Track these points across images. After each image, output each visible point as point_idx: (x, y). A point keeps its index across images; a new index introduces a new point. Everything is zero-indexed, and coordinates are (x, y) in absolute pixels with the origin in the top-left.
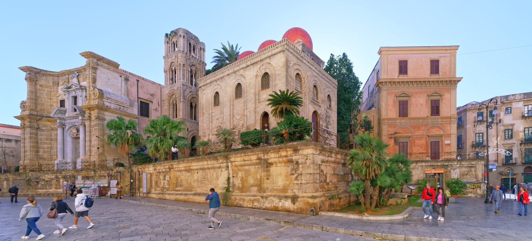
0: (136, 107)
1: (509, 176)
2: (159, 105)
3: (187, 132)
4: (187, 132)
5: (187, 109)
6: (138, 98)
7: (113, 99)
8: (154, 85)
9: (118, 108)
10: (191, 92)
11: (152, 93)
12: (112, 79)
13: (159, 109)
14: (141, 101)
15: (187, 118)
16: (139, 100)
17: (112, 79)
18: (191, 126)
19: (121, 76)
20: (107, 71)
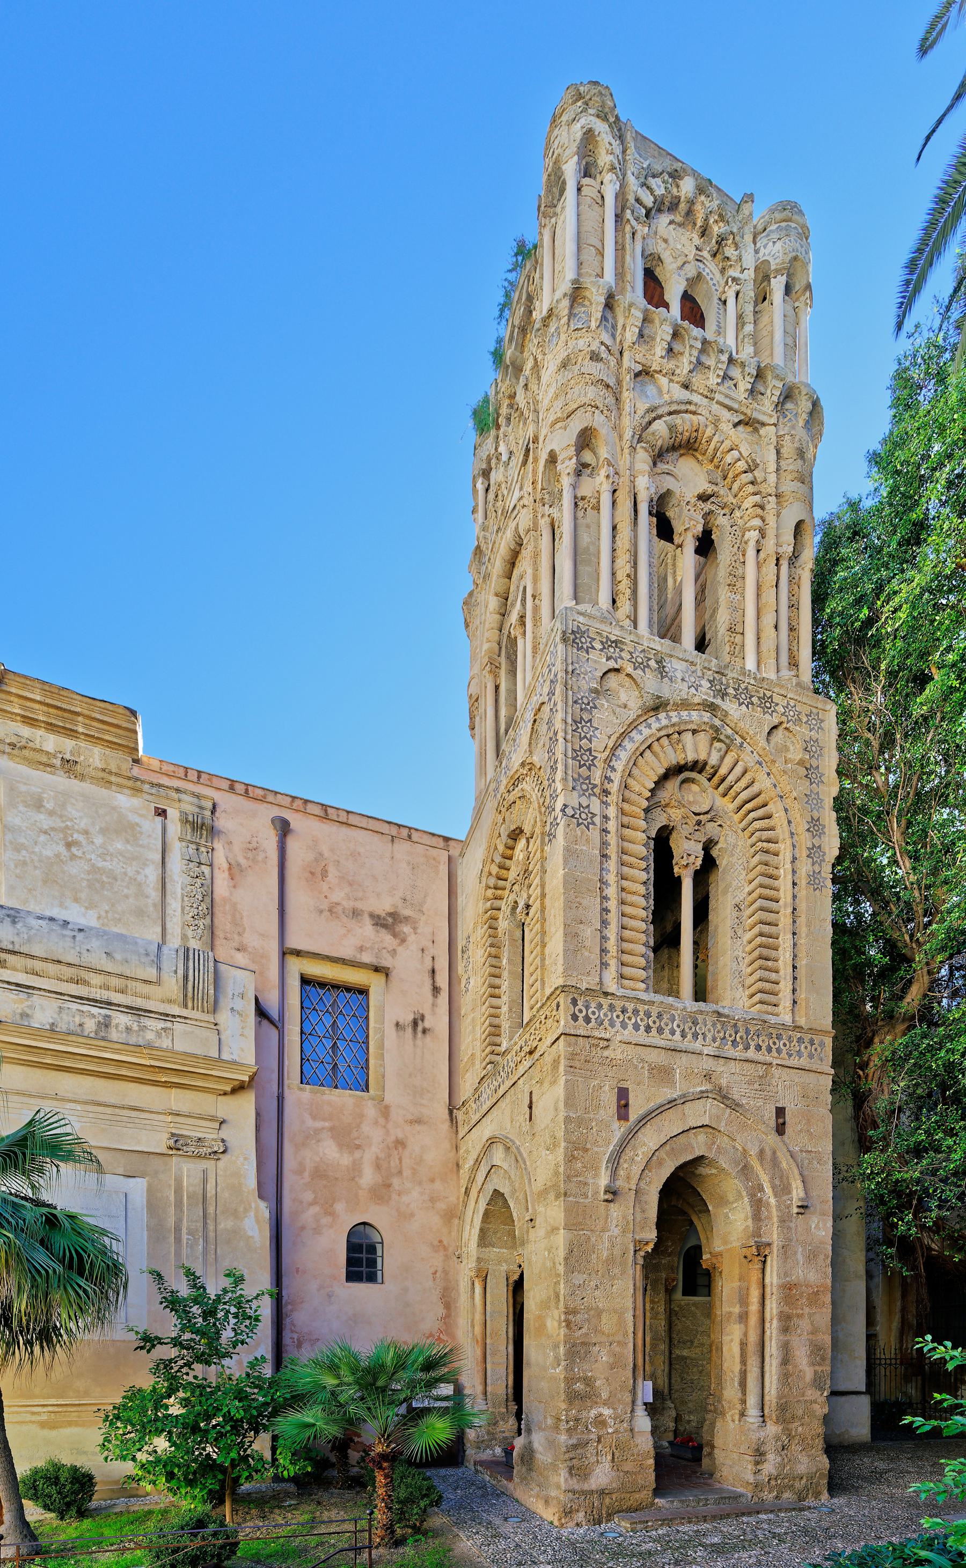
0: (239, 1004)
1: (367, 1259)
2: (436, 990)
3: (618, 1130)
4: (618, 1130)
5: (611, 891)
6: (285, 953)
7: (37, 950)
8: (402, 848)
9: (90, 1026)
10: (658, 706)
11: (384, 906)
12: (98, 840)
13: (438, 1021)
14: (305, 981)
15: (612, 987)
16: (296, 967)
17: (98, 840)
18: (654, 1057)
19: (162, 813)
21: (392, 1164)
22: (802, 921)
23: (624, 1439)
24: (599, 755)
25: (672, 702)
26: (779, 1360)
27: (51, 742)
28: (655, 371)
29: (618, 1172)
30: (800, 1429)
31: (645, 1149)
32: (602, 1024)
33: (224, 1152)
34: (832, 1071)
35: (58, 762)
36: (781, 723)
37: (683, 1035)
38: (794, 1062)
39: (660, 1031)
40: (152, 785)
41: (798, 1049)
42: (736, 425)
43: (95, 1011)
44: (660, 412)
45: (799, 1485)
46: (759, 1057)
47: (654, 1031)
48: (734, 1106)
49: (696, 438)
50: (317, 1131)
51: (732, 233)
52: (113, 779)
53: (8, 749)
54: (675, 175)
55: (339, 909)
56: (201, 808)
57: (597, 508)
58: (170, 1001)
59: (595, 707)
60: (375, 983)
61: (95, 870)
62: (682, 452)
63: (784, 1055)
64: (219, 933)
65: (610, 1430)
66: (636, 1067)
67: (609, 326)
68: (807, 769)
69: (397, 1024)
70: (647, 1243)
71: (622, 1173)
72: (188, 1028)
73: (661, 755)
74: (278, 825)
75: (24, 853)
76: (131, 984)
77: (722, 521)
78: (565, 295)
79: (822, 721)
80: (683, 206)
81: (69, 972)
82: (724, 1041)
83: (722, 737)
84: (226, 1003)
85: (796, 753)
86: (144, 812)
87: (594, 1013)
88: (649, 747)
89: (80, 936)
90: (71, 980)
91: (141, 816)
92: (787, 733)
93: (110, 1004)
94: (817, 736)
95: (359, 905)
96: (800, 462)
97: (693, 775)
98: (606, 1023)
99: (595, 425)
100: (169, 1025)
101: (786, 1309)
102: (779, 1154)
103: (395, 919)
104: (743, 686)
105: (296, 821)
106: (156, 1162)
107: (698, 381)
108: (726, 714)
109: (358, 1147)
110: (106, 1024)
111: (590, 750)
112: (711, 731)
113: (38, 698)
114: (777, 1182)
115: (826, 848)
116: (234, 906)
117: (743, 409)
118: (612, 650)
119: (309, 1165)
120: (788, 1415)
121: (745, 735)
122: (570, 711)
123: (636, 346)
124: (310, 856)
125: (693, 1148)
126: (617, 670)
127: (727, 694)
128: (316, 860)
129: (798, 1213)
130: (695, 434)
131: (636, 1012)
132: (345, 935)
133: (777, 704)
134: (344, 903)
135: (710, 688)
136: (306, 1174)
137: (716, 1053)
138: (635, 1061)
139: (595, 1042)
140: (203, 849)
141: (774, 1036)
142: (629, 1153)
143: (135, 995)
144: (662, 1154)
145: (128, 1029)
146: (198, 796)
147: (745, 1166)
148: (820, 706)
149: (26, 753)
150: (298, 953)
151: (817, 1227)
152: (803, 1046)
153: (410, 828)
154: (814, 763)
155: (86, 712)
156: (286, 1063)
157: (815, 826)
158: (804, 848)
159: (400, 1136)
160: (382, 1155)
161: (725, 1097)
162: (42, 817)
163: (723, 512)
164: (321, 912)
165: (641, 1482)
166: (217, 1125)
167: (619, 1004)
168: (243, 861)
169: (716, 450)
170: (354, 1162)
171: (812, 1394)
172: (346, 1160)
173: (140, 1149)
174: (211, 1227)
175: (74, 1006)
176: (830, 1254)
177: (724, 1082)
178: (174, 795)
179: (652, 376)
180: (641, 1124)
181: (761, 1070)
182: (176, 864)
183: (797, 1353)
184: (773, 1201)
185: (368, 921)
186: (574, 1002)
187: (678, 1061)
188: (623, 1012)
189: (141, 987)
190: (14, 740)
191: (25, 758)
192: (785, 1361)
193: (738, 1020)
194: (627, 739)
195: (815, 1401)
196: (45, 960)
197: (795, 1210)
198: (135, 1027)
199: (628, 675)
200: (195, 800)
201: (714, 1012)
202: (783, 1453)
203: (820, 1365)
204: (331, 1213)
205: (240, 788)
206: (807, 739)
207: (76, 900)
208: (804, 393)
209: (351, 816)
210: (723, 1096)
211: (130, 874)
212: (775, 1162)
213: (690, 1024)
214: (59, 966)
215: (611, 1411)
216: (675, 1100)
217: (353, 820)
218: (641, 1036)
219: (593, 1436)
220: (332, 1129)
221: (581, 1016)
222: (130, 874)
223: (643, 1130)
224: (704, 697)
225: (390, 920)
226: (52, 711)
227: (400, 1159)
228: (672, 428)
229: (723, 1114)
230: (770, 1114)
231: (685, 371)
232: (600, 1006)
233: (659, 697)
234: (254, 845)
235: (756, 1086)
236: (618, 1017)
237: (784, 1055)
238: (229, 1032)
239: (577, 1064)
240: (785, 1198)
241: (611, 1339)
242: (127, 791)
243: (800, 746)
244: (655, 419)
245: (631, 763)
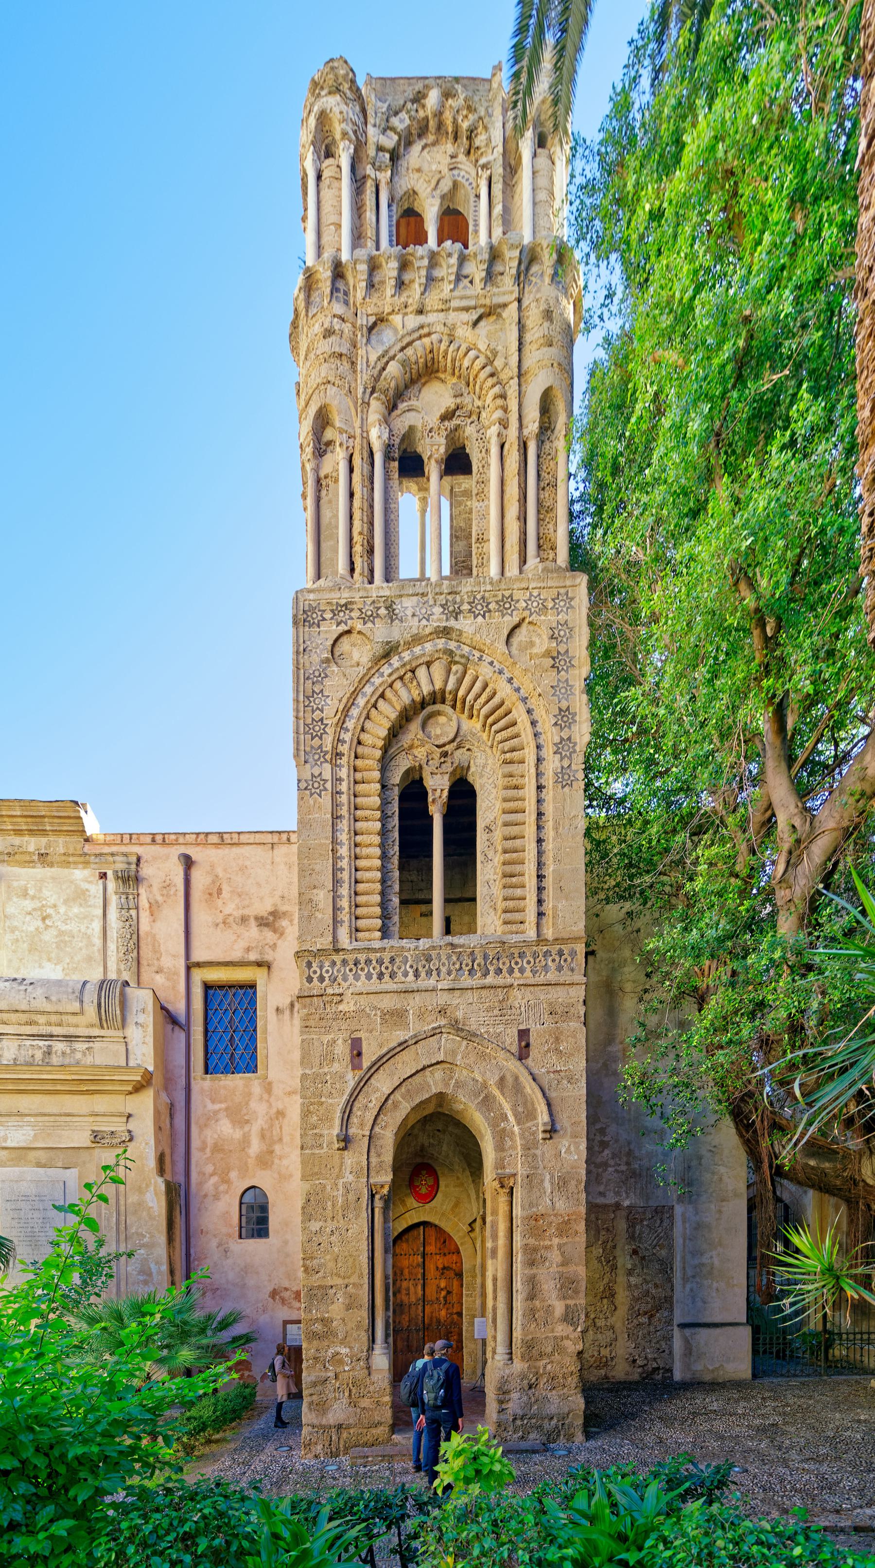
0: (141, 1018)
3: (351, 1079)
9: (39, 1055)
11: (263, 908)
18: (388, 1003)
20: (39, 871)
21: (274, 1133)
22: (549, 826)
23: (360, 1377)
24: (329, 722)
25: (402, 643)
26: (524, 1295)
27: (32, 844)
28: (389, 314)
29: (351, 1121)
30: (549, 1367)
31: (378, 1094)
32: (335, 980)
33: (131, 1140)
34: (584, 980)
35: (36, 858)
36: (523, 619)
37: (417, 975)
38: (541, 979)
39: (392, 976)
40: (96, 855)
41: (544, 963)
42: (475, 324)
43: (41, 1043)
44: (391, 353)
45: (547, 1426)
46: (499, 981)
47: (387, 977)
48: (470, 1036)
49: (433, 359)
50: (216, 1112)
51: (480, 118)
52: (71, 859)
53: (6, 858)
54: (419, 98)
55: (231, 919)
56: (129, 863)
57: (336, 481)
58: (92, 1026)
59: (326, 676)
60: (258, 976)
61: (61, 933)
62: (423, 381)
63: (528, 973)
64: (144, 962)
65: (347, 1368)
66: (369, 1016)
67: (341, 295)
68: (553, 658)
69: (278, 1009)
70: (382, 1186)
71: (355, 1120)
72: (104, 1045)
73: (394, 699)
74: (182, 859)
75: (17, 933)
76: (64, 1017)
77: (470, 431)
78: (300, 288)
79: (572, 599)
80: (432, 124)
81: (24, 1017)
82: (461, 972)
83: (457, 659)
84: (131, 1019)
85: (542, 644)
86: (92, 879)
87: (327, 971)
88: (382, 696)
89: (30, 988)
91: (90, 882)
92: (531, 628)
93: (52, 1036)
94: (566, 617)
95: (246, 912)
96: (546, 324)
97: (438, 707)
98: (339, 979)
99: (328, 401)
100: (91, 1044)
101: (532, 1241)
102: (522, 1079)
103: (275, 917)
104: (478, 597)
105: (194, 853)
106: (84, 1155)
107: (433, 300)
108: (461, 633)
109: (247, 1122)
110: (48, 1053)
111: (322, 720)
112: (445, 657)
113: (19, 813)
114: (520, 1109)
115: (576, 738)
116: (154, 937)
117: (482, 301)
118: (342, 614)
119: (210, 1142)
121: (482, 647)
122: (301, 689)
123: (367, 300)
124: (209, 880)
125: (429, 1086)
126: (349, 632)
127: (461, 612)
128: (214, 882)
129: (544, 1139)
130: (431, 356)
131: (368, 962)
132: (236, 941)
133: (518, 601)
134: (235, 913)
135: (443, 613)
136: (208, 1150)
137: (450, 987)
138: (367, 1009)
139: (329, 999)
140: (131, 897)
141: (516, 955)
142: (362, 1100)
143: (68, 1025)
144: (397, 1096)
145: (63, 1053)
146: (125, 855)
147: (486, 1097)
148: (568, 583)
149: (17, 857)
150: (198, 965)
151: (568, 1150)
152: (550, 959)
153: (288, 832)
154: (562, 648)
155: (48, 814)
156: (192, 1059)
157: (565, 717)
158: (551, 745)
159: (280, 1107)
160: (266, 1126)
161: (458, 1029)
162: (27, 902)
163: (469, 421)
164: (217, 925)
165: (377, 1418)
166: (125, 1119)
167: (351, 958)
168: (160, 899)
169: (454, 360)
170: (244, 1134)
171: (561, 1329)
172: (238, 1134)
173: (72, 1145)
174: (122, 1202)
175: (28, 1043)
176: (584, 1178)
177: (460, 1015)
178: (111, 859)
179: (387, 320)
180: (373, 1070)
181: (500, 993)
182: (113, 913)
183: (545, 1287)
184: (516, 1129)
185: (253, 923)
186: (309, 965)
187: (411, 1002)
188: (355, 965)
190: (10, 850)
191: (17, 861)
192: (531, 1297)
193: (474, 947)
194: (360, 695)
196: (8, 1011)
197: (541, 1136)
198: (68, 1051)
199: (359, 632)
200: (124, 859)
201: (447, 944)
202: (530, 1392)
203: (572, 1298)
204: (226, 1181)
205: (159, 838)
206: (554, 625)
207: (49, 960)
208: (545, 246)
209: (242, 836)
210: (457, 1027)
211: (83, 930)
212: (518, 1087)
213: (424, 962)
214: (18, 1014)
215: (348, 1350)
216: (406, 1041)
217: (244, 838)
218: (374, 985)
219: (331, 1374)
220: (227, 1109)
221: (315, 976)
222: (83, 930)
223: (375, 1076)
224: (435, 624)
225: (271, 918)
226: (29, 820)
227: (281, 1128)
228: (404, 363)
229: (460, 1045)
230: (511, 1039)
231: (417, 296)
232: (334, 963)
233: (388, 643)
234: (168, 882)
235: (496, 1012)
236: (351, 970)
237: (528, 973)
238: (134, 1042)
239: (311, 1023)
240: (529, 1124)
241: (346, 1281)
242: (80, 866)
243: (545, 634)
244: (387, 363)
245: (364, 716)
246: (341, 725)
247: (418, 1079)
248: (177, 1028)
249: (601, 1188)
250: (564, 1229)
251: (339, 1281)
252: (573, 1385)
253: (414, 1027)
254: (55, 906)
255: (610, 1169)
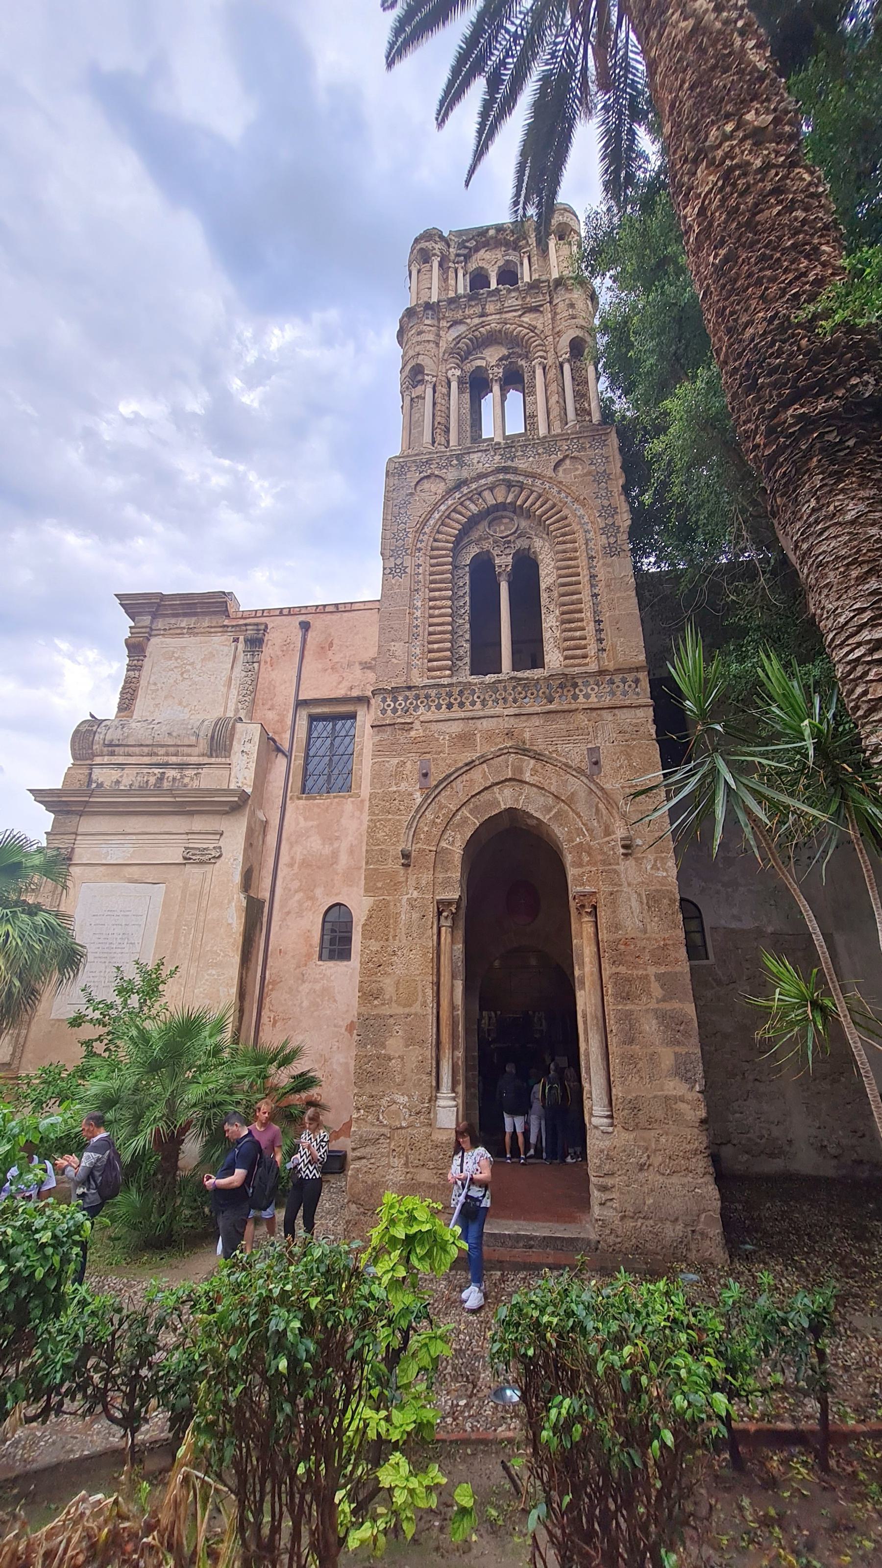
9: (152, 780)
30: (663, 1140)
39: (462, 705)
43: (156, 771)
58: (203, 755)
90: (148, 755)
98: (411, 711)
109: (337, 838)
120: (642, 1118)
144: (465, 811)
167: (423, 692)
172: (327, 850)
180: (441, 787)
185: (357, 667)
189: (186, 750)
195: (682, 1099)
216: (473, 761)
217: (355, 607)
218: (444, 713)
236: (400, 704)
241: (407, 1010)
246: (420, 531)
247: (486, 795)
248: (280, 755)
249: (735, 911)
250: (660, 955)
251: (400, 1010)
252: (700, 1171)
253: (482, 748)
254: (193, 663)
255: (742, 889)
